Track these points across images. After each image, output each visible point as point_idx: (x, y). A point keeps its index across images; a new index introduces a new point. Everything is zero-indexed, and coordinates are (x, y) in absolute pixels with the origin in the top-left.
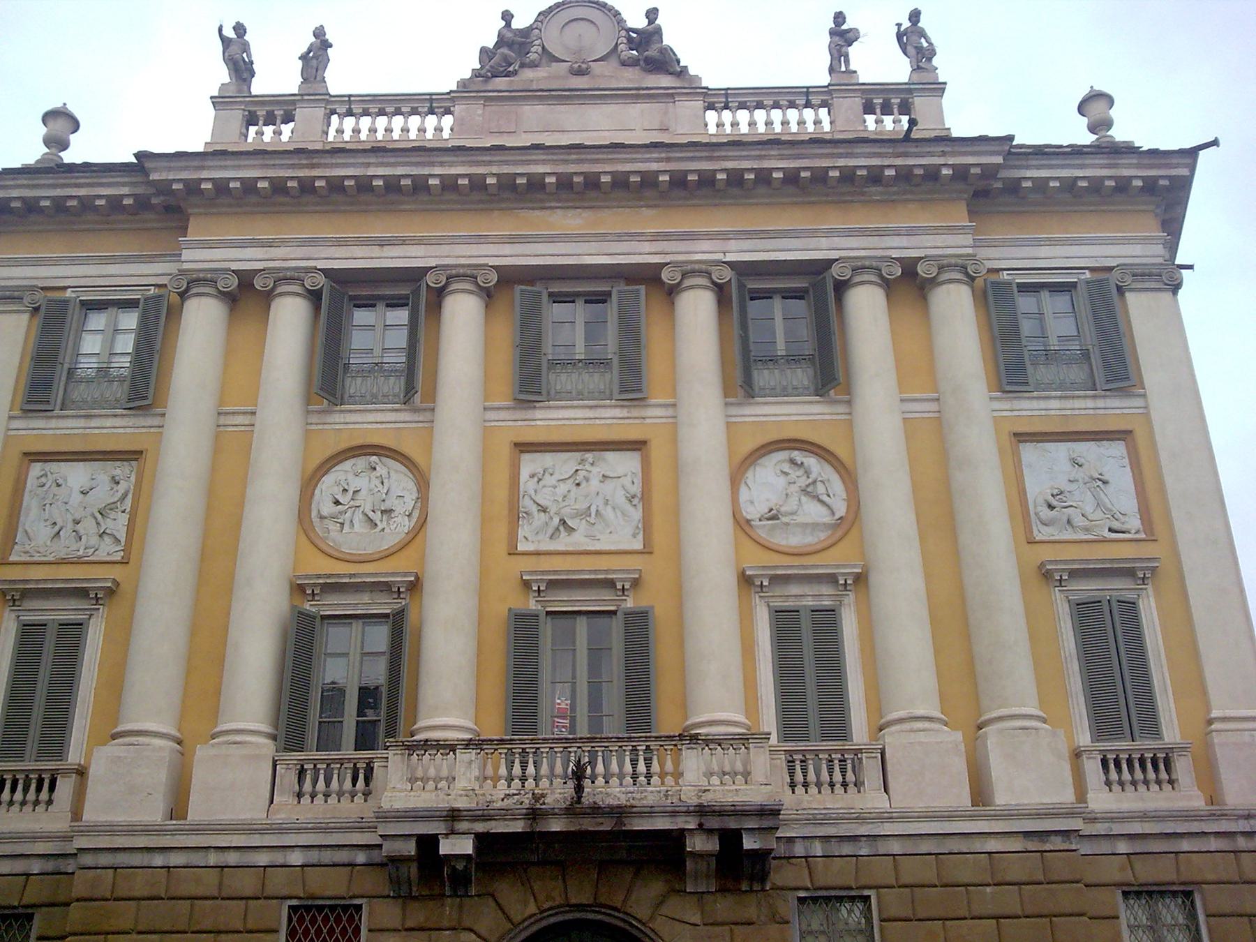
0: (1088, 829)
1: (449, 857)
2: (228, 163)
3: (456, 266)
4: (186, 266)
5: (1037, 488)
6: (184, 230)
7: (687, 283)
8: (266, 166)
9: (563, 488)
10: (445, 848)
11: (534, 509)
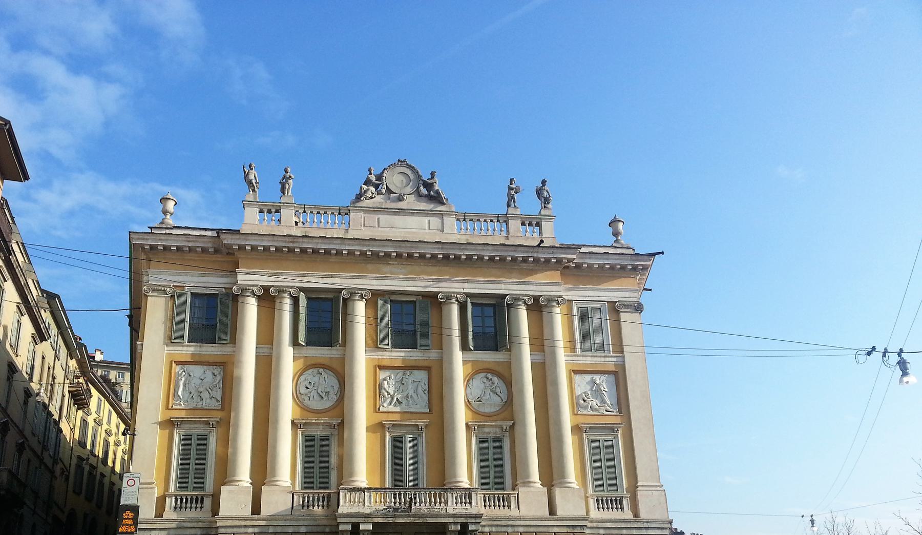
0: (589, 525)
10: (362, 527)
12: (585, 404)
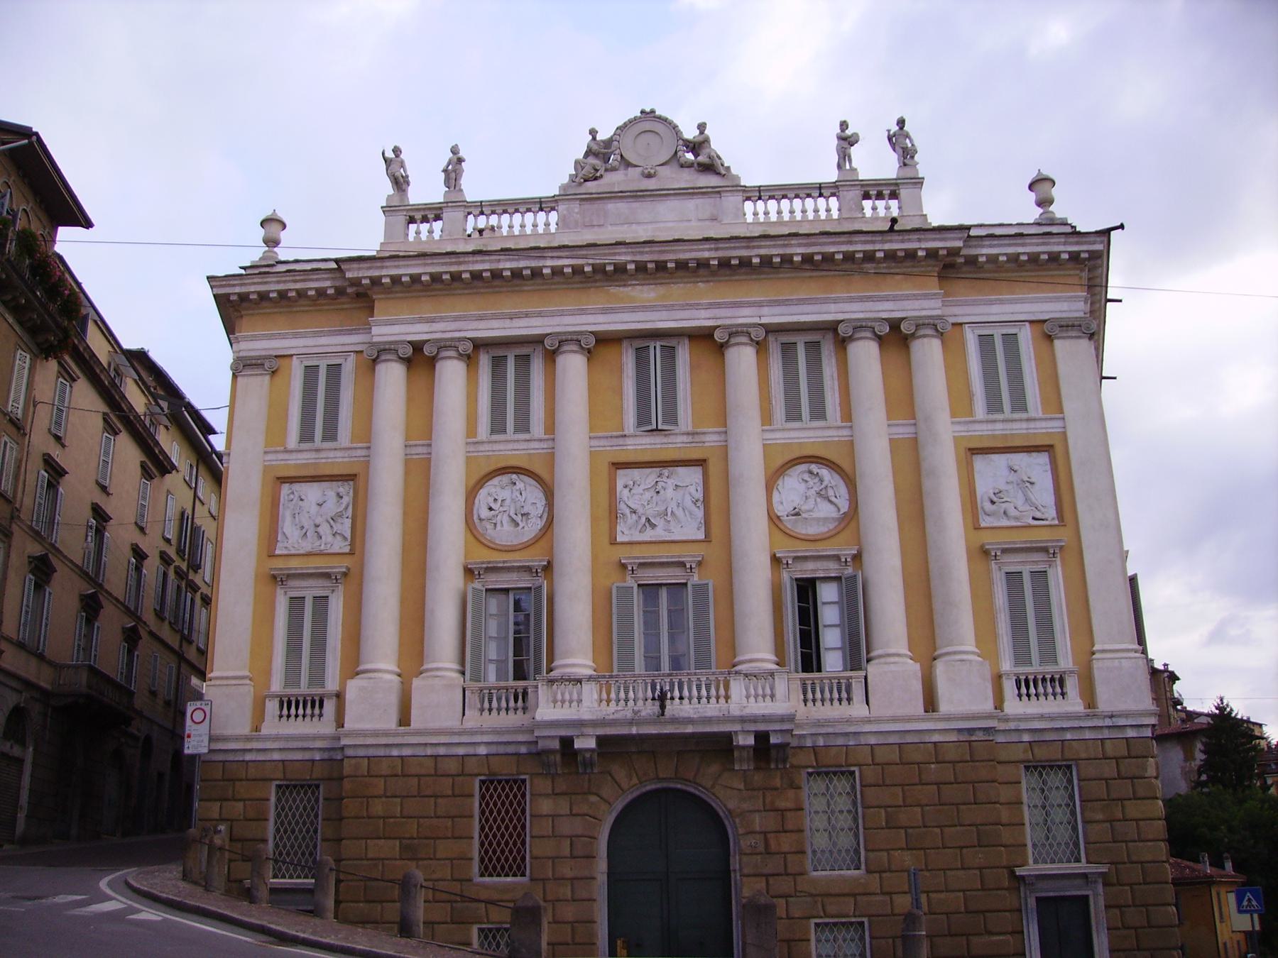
0: (1002, 726)
1: (581, 750)
2: (401, 263)
3: (565, 333)
4: (375, 339)
5: (984, 488)
6: (371, 310)
7: (733, 341)
8: (426, 265)
9: (647, 495)
11: (627, 511)
12: (994, 507)
